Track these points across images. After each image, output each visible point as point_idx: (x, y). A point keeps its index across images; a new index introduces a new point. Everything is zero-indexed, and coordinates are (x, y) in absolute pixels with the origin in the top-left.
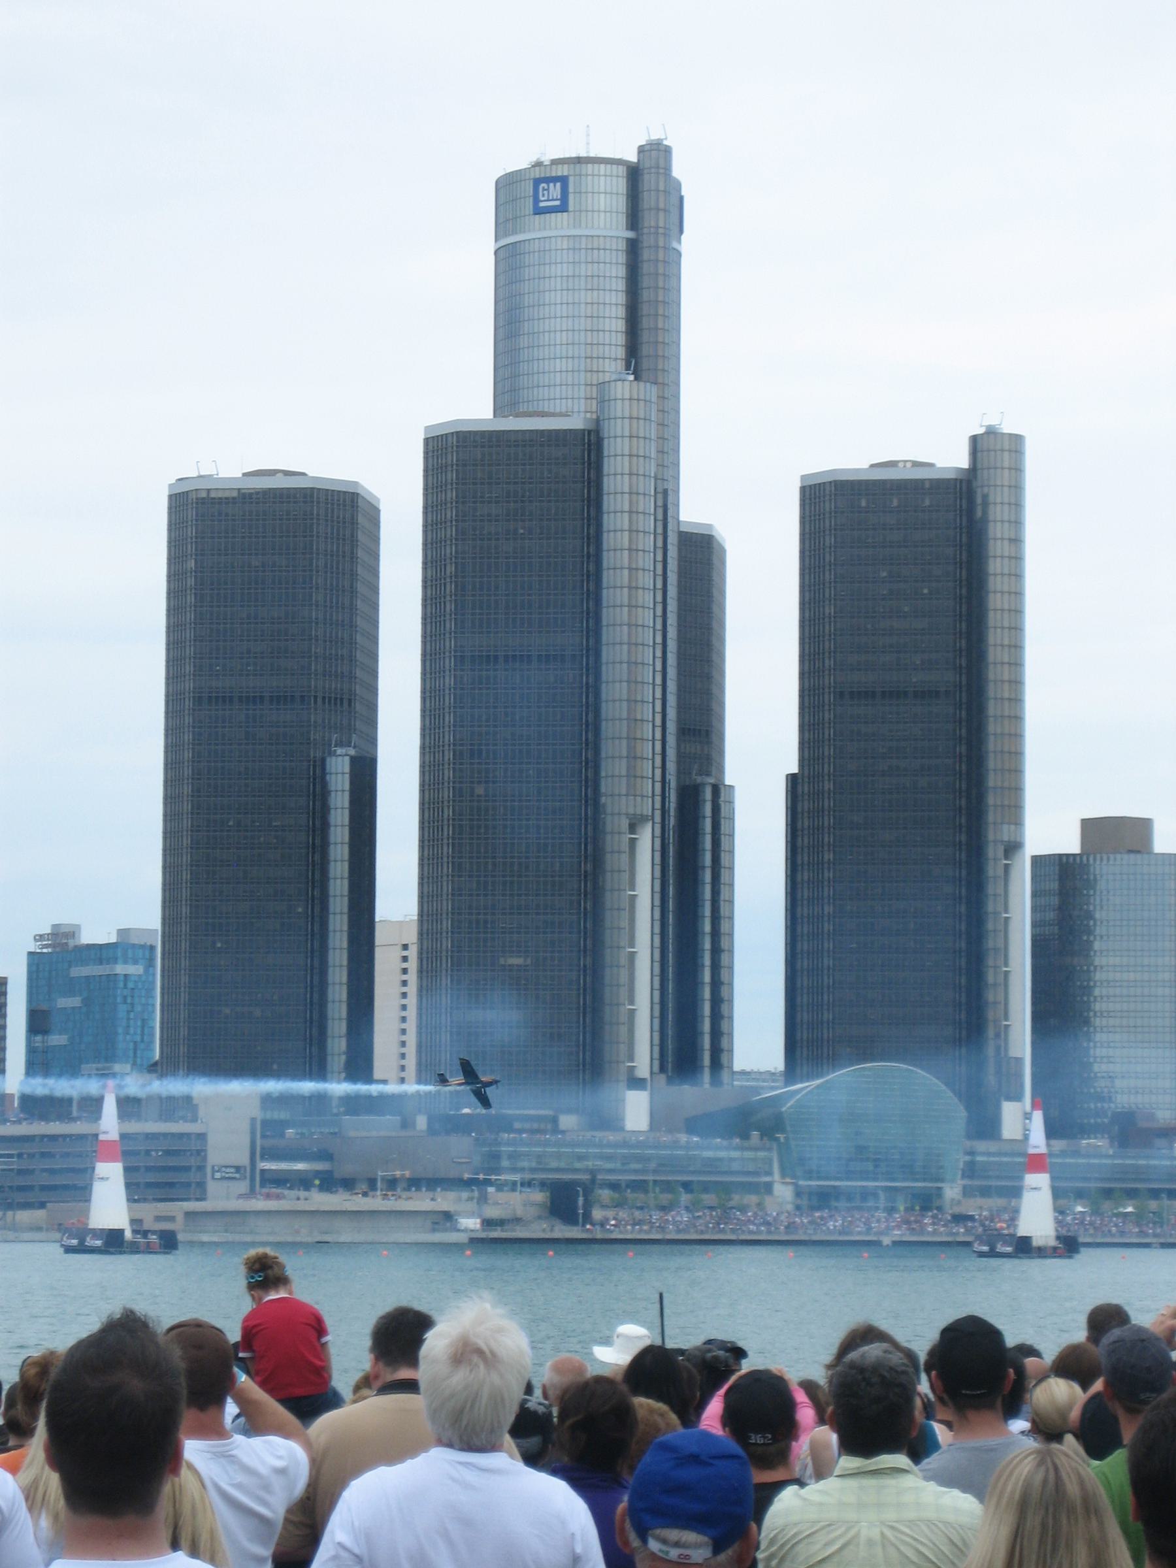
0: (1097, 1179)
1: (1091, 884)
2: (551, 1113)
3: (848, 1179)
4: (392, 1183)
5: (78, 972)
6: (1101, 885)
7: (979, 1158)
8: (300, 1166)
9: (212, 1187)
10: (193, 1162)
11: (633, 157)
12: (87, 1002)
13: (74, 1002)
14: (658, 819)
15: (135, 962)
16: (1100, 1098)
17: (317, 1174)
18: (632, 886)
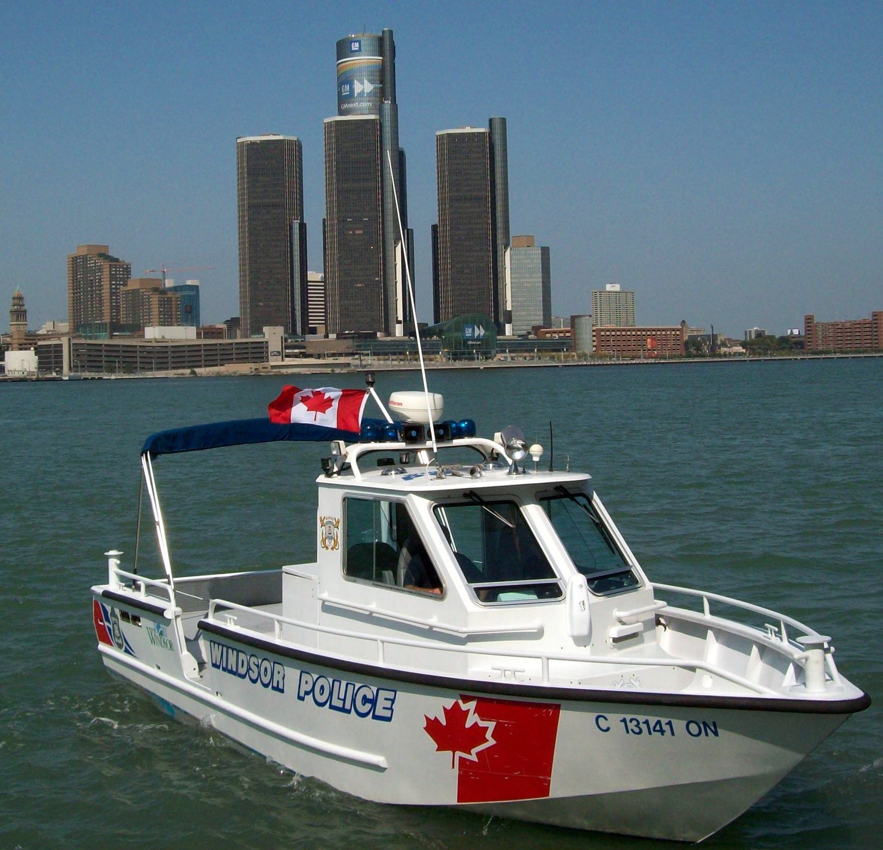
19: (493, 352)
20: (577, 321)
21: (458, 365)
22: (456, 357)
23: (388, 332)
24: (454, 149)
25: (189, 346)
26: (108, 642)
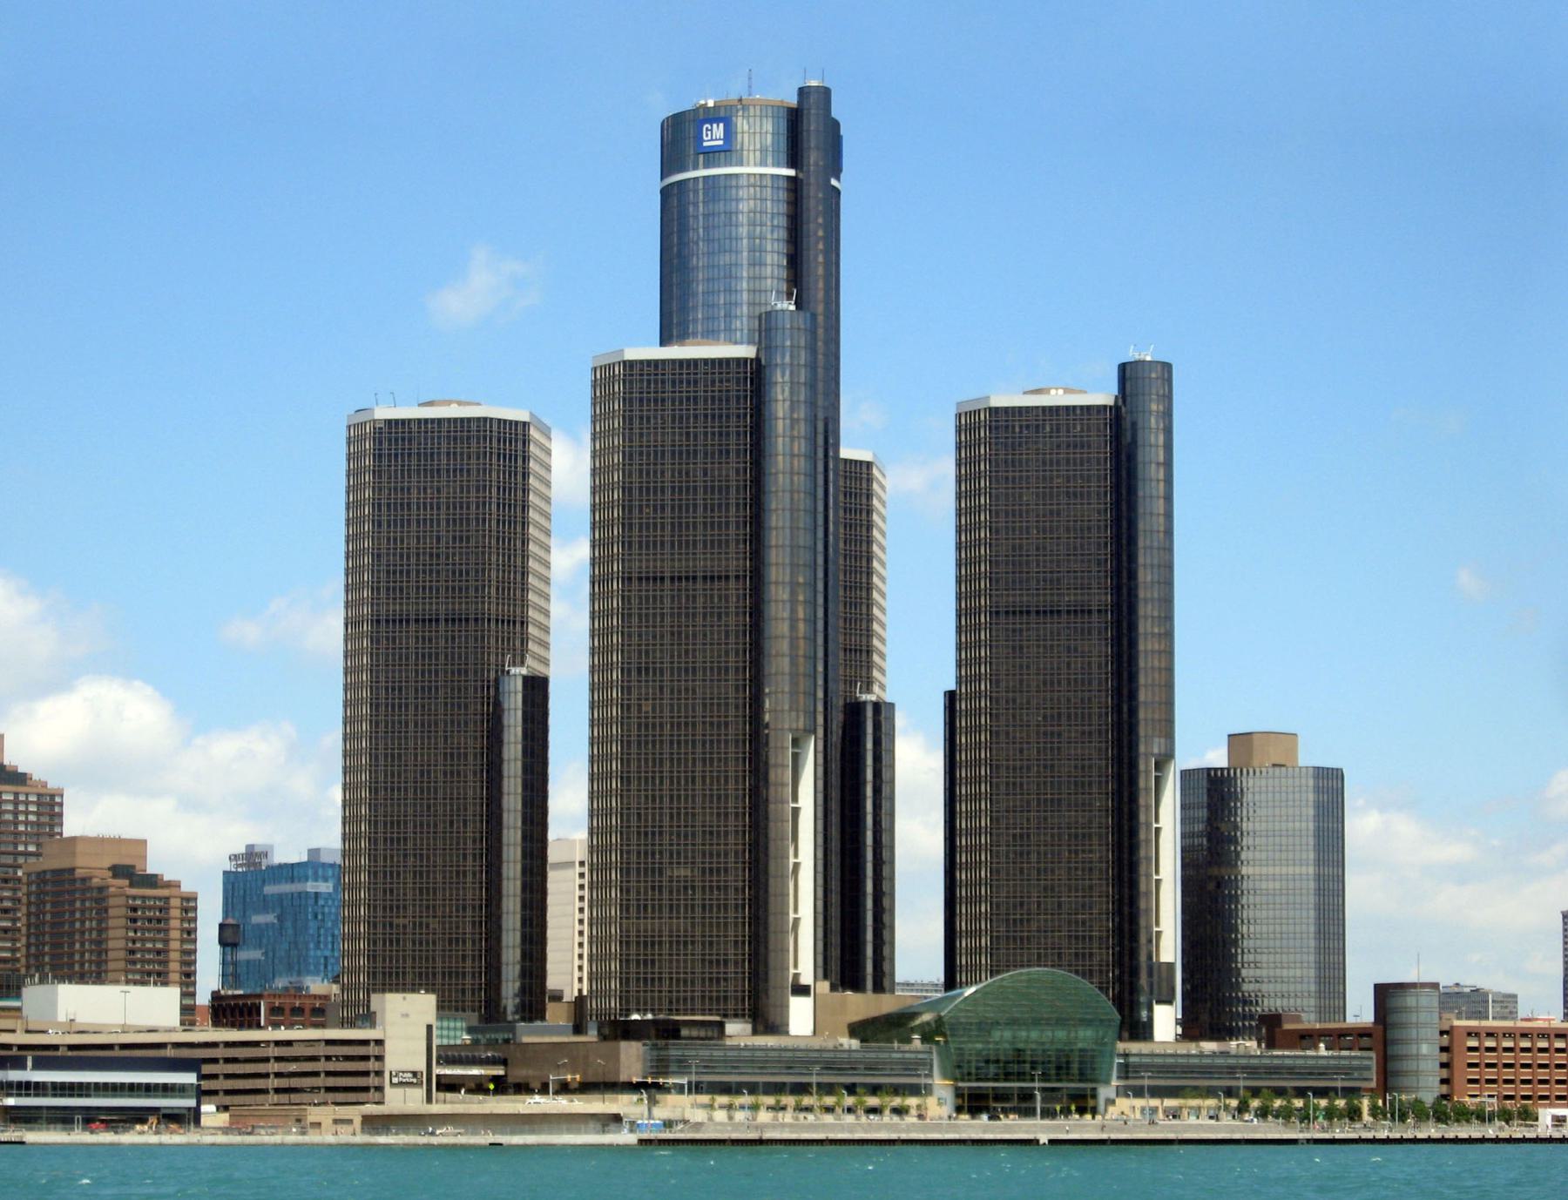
1: (1236, 796)
2: (717, 1018)
3: (1006, 1080)
5: (269, 889)
6: (1248, 797)
7: (1132, 1059)
8: (475, 1071)
9: (389, 1091)
10: (372, 1065)
12: (280, 918)
13: (270, 918)
14: (820, 732)
15: (326, 880)
16: (1245, 1002)
17: (495, 1079)
18: (795, 799)
19: (1105, 1092)
20: (1395, 1002)
21: (979, 1127)
22: (972, 1103)
23: (767, 1020)
24: (997, 447)
25: (124, 1046)
26: (788, 177)
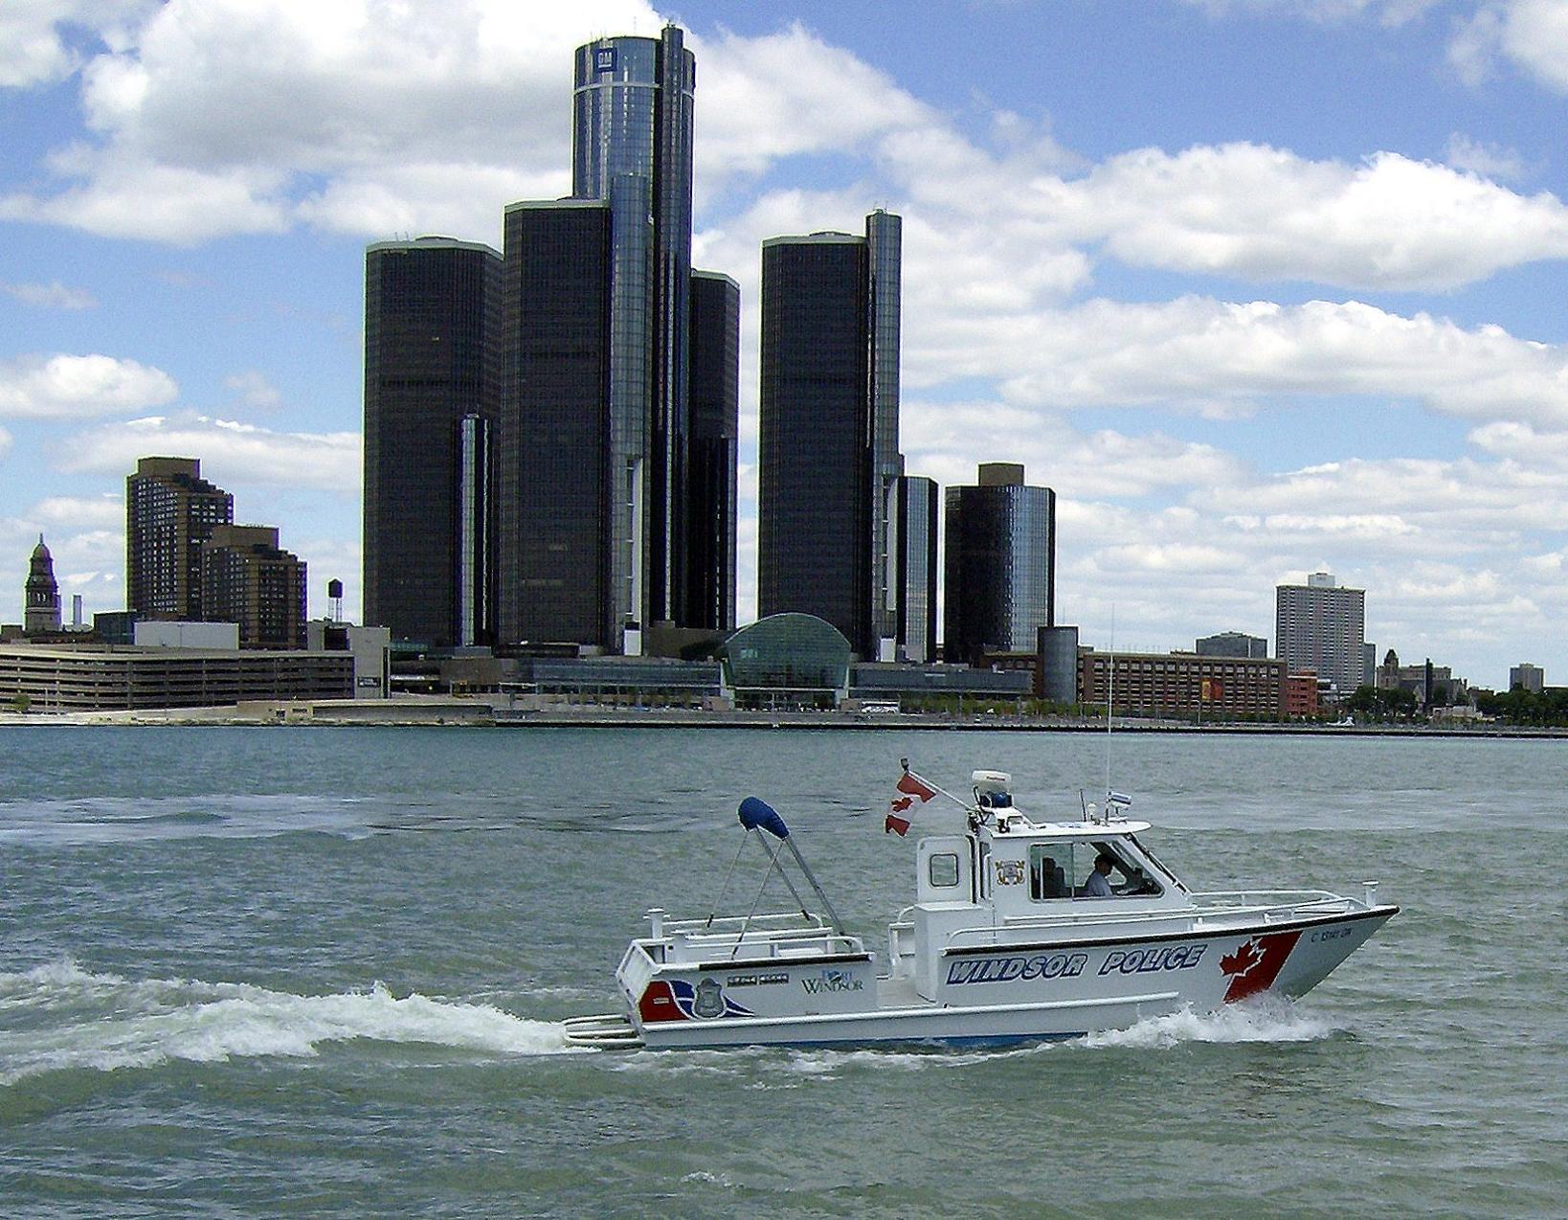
0: (331, 446)
4: (463, 689)
10: (346, 674)
11: (659, 37)
17: (432, 683)
23: (610, 645)
